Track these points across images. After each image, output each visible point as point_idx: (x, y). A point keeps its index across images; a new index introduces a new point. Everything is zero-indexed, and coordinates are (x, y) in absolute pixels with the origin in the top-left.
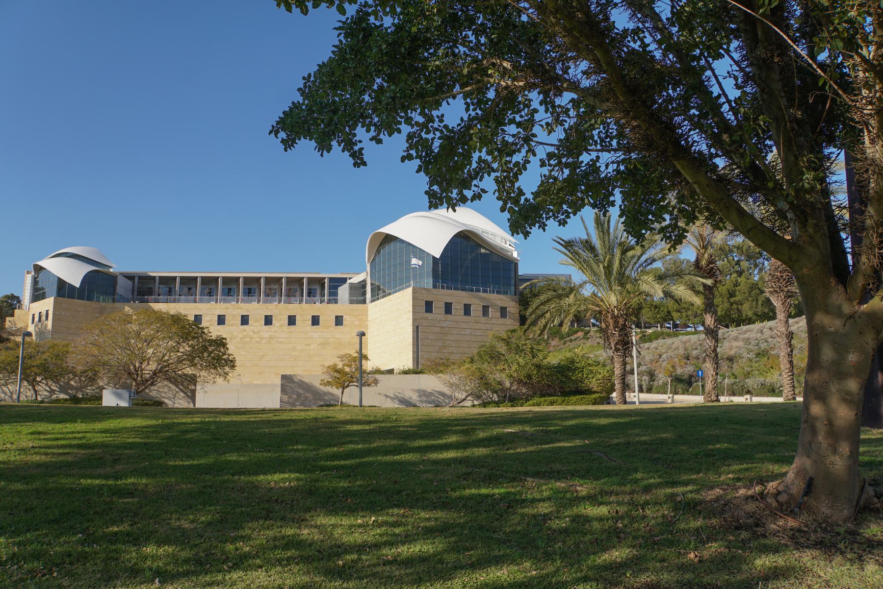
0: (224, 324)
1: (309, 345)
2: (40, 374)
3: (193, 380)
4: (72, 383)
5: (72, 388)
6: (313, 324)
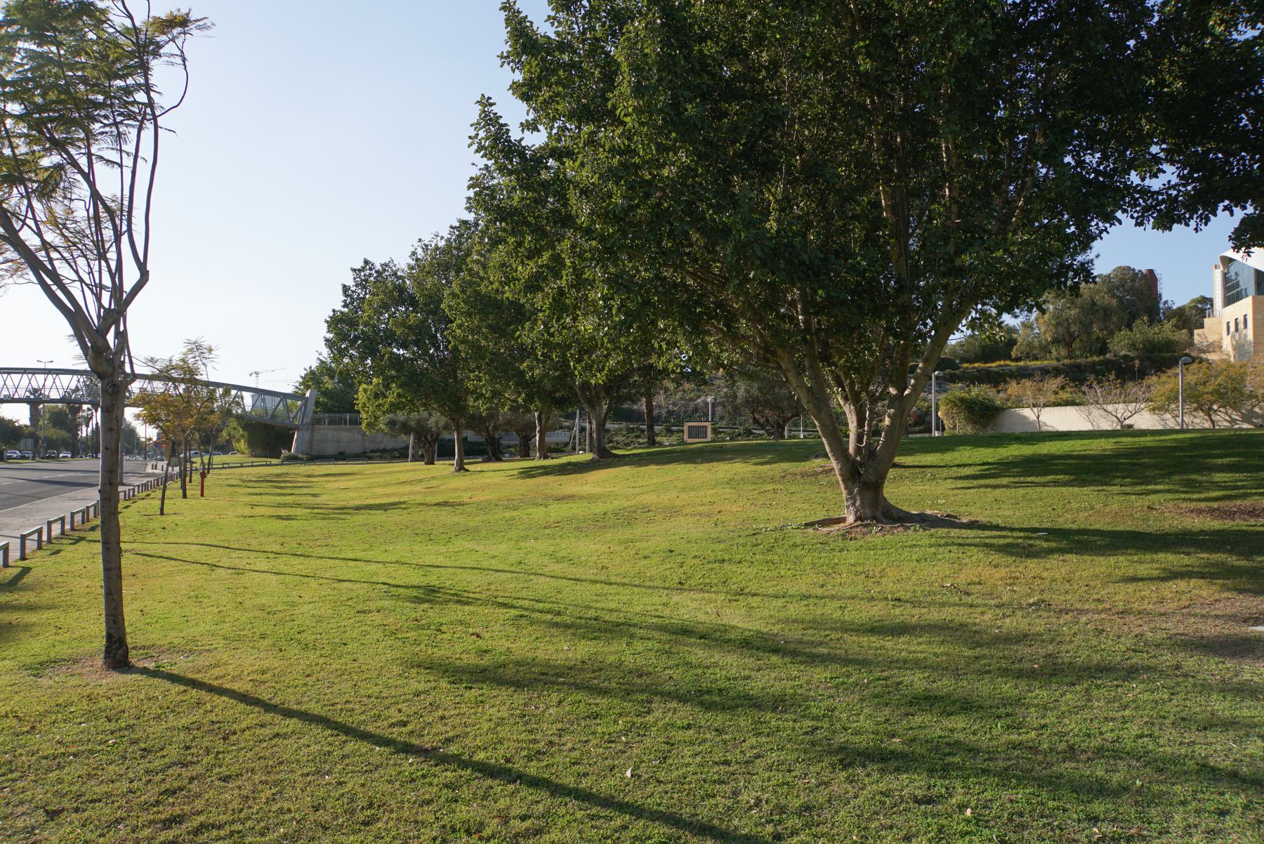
2: (1214, 402)
4: (1257, 410)
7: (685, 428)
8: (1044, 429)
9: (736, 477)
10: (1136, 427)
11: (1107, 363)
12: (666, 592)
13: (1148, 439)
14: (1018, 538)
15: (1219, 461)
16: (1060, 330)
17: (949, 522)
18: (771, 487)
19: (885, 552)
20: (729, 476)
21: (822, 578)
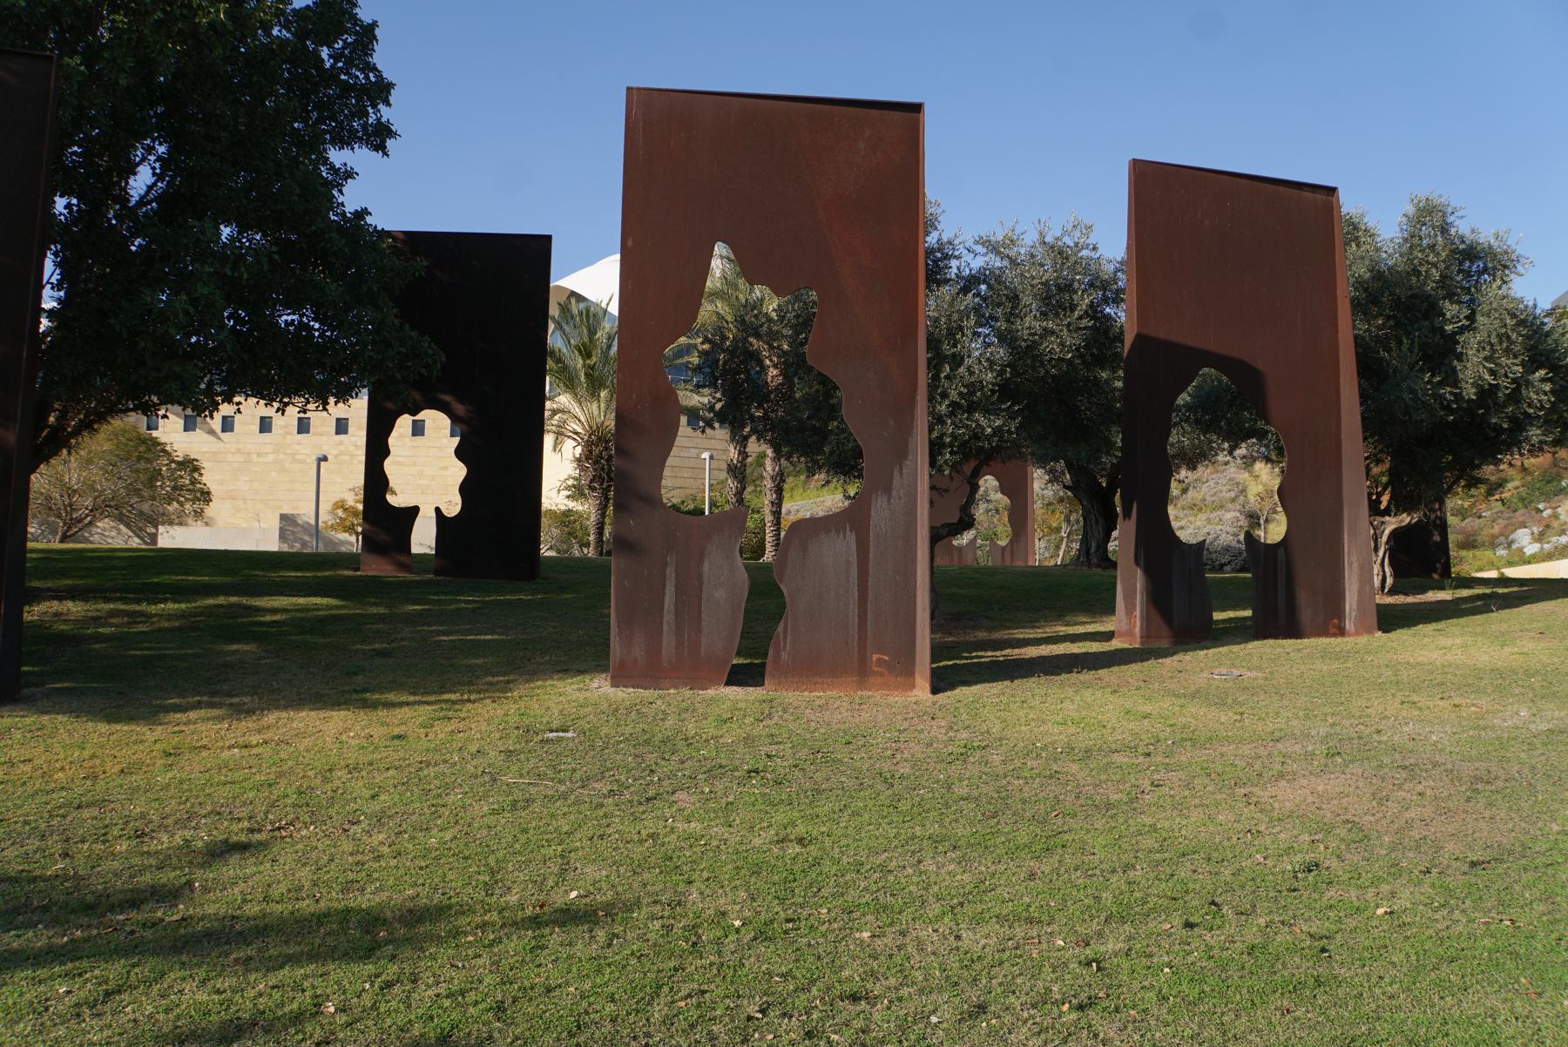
0: (308, 432)
1: (445, 468)
6: (262, 431)
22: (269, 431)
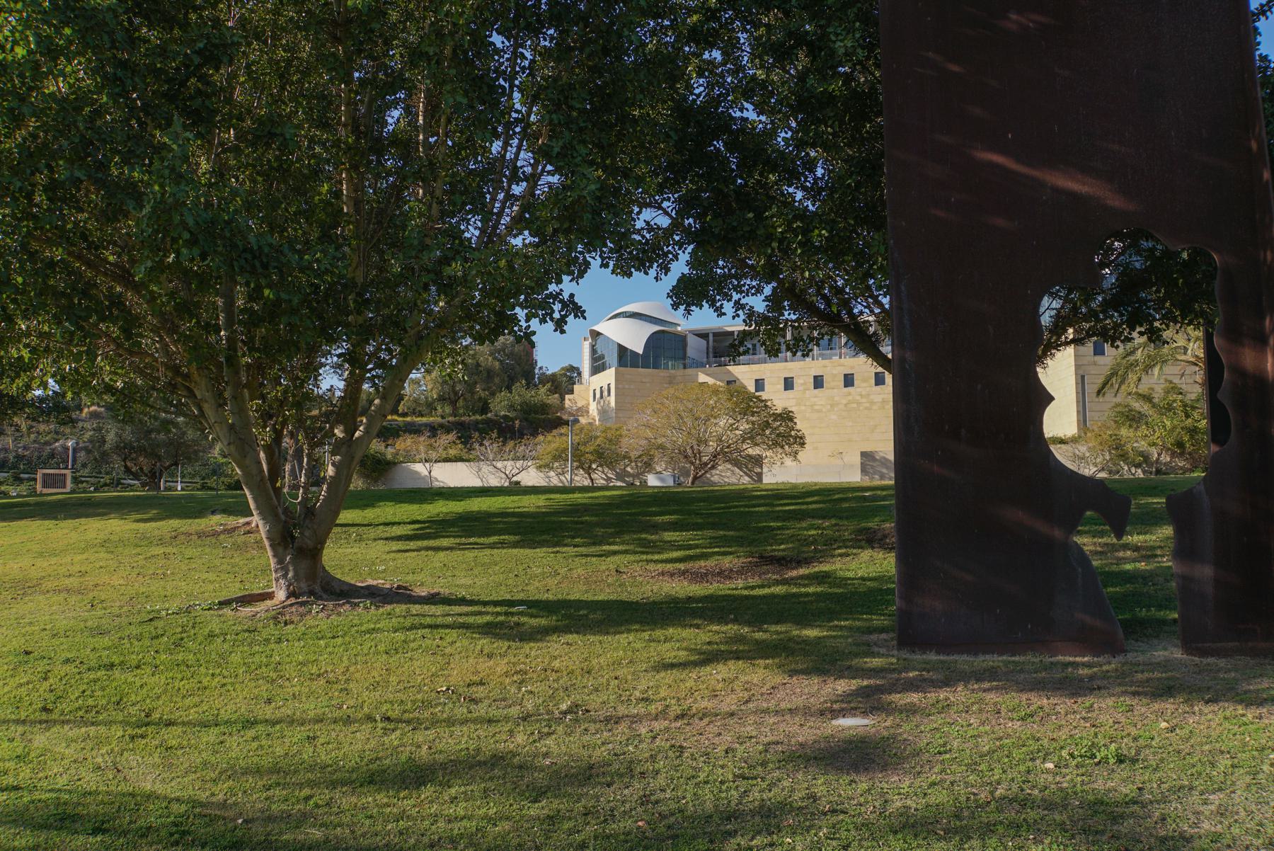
2: (595, 461)
3: (758, 461)
4: (629, 469)
5: (629, 475)
6: (877, 384)
7: (39, 476)
8: (436, 484)
9: (112, 537)
10: (523, 484)
11: (488, 422)
12: (20, 729)
13: (576, 495)
14: (498, 614)
15: (659, 519)
16: (447, 388)
17: (400, 595)
18: (159, 550)
19: (339, 641)
20: (102, 536)
21: (263, 689)
22: (852, 385)
